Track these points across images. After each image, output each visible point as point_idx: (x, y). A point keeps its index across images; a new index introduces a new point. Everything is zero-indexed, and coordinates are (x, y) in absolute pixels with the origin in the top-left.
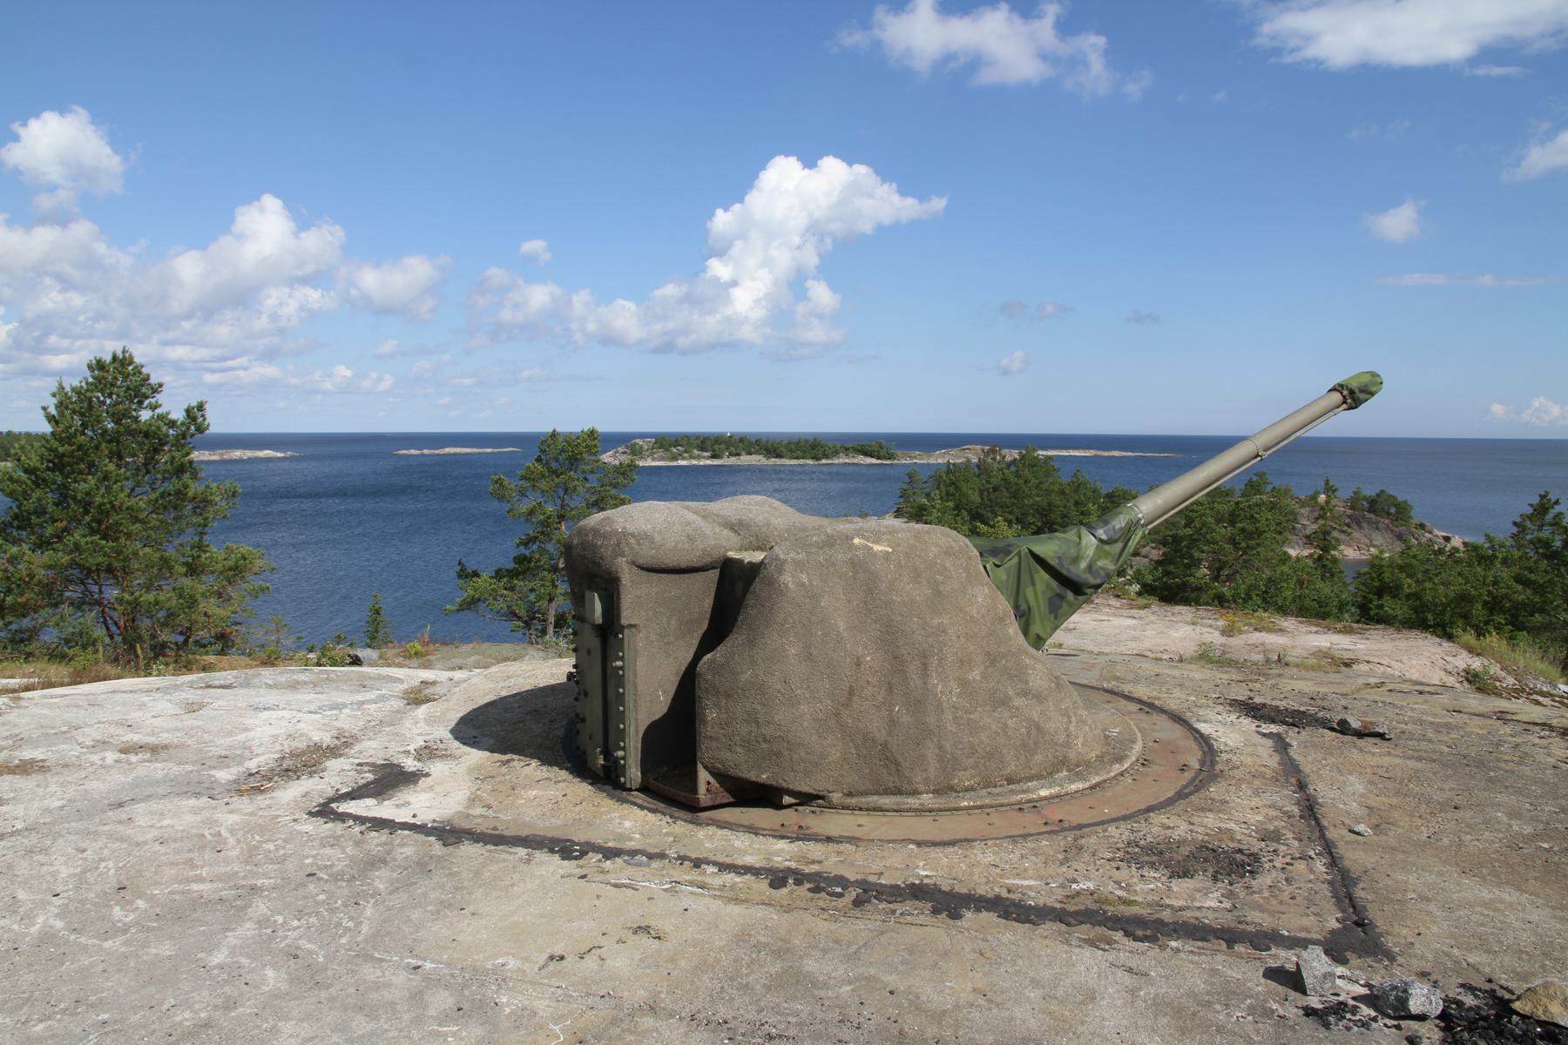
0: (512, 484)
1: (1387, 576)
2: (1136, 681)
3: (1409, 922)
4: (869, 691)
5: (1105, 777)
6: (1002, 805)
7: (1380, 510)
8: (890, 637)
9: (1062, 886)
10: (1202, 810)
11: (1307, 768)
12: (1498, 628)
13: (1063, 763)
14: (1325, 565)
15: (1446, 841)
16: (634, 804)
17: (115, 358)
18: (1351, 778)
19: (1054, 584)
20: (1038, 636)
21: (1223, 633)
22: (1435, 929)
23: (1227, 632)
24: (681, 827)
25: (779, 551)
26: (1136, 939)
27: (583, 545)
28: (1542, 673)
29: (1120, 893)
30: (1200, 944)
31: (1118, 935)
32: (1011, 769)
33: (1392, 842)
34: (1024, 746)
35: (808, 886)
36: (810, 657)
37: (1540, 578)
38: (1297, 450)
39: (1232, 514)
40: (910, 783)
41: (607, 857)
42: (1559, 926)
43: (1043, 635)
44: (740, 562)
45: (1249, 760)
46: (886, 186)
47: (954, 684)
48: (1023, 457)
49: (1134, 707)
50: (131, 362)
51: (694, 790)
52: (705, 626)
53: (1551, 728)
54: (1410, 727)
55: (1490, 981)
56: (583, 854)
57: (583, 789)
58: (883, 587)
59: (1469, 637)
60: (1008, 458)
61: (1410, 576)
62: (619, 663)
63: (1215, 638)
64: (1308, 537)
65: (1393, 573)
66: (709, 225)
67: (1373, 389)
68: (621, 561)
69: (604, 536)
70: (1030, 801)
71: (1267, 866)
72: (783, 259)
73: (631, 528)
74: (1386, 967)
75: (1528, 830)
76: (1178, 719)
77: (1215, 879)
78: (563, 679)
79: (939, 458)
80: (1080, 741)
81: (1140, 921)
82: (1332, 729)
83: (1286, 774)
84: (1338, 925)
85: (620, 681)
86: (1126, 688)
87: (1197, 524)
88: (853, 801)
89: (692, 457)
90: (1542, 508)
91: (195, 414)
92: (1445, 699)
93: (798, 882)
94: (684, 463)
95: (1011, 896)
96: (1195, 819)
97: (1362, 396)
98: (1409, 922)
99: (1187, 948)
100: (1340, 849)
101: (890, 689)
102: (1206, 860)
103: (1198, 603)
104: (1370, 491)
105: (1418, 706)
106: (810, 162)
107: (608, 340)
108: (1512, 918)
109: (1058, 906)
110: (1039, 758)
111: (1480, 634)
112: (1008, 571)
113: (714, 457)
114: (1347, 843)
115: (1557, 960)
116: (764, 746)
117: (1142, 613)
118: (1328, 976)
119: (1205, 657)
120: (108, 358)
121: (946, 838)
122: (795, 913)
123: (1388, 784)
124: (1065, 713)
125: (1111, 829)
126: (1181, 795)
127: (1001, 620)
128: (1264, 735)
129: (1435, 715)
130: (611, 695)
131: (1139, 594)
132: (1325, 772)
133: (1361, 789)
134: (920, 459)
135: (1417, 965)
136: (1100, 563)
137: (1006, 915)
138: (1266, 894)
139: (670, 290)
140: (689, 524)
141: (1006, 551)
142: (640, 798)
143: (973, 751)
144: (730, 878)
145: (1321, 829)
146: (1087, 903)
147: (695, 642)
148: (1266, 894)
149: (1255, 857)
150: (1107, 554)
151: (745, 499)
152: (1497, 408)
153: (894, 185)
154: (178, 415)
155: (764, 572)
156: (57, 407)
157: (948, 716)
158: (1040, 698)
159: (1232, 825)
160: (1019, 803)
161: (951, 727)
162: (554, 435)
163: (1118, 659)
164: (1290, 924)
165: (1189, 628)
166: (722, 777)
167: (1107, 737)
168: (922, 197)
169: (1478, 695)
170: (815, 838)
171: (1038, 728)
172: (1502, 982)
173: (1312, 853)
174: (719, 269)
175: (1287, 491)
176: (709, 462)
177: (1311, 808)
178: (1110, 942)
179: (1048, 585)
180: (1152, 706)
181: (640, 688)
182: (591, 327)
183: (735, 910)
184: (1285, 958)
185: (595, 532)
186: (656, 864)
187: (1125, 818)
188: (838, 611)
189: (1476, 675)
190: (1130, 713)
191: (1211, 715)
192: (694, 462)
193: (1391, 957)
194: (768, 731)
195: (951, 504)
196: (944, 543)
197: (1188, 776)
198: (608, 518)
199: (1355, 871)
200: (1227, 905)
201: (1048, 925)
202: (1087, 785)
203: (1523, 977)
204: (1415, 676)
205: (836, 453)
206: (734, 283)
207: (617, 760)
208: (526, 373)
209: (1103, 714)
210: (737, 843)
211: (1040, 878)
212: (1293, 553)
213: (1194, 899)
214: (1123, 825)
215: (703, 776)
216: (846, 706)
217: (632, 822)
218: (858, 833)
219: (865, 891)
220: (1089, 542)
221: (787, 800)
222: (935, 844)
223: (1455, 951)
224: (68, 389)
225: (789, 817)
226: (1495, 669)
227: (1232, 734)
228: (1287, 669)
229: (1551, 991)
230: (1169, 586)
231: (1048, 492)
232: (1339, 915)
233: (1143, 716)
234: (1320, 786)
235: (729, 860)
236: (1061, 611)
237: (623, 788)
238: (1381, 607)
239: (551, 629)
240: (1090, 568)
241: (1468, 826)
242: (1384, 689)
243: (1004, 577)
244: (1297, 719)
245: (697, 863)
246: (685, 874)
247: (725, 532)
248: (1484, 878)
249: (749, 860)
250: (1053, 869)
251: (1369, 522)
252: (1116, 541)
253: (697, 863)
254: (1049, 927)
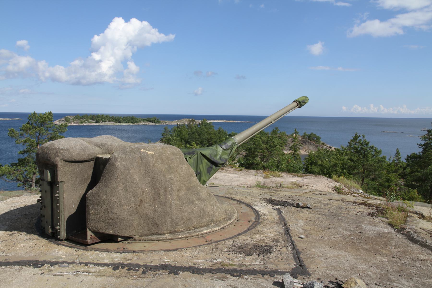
0: (17, 132)
1: (313, 159)
2: (236, 194)
3: (315, 264)
4: (147, 201)
5: (225, 225)
6: (192, 236)
7: (311, 139)
8: (154, 182)
9: (211, 261)
10: (255, 234)
11: (287, 219)
12: (344, 174)
13: (212, 221)
14: (295, 156)
15: (326, 238)
16: (63, 245)
18: (300, 221)
19: (209, 163)
20: (204, 180)
21: (264, 178)
22: (322, 265)
23: (265, 178)
24: (81, 252)
25: (116, 154)
26: (234, 276)
27: (43, 153)
28: (355, 187)
29: (229, 262)
30: (254, 276)
31: (229, 276)
32: (195, 224)
33: (311, 240)
35: (126, 268)
36: (126, 190)
37: (355, 159)
38: (284, 120)
39: (267, 140)
40: (162, 231)
41: (52, 266)
42: (355, 261)
43: (205, 180)
44: (102, 158)
45: (270, 217)
46: (154, 30)
47: (175, 197)
48: (202, 123)
49: (235, 202)
51: (86, 238)
52: (90, 181)
53: (356, 203)
54: (317, 205)
55: (337, 279)
56: (42, 265)
57: (44, 241)
58: (151, 165)
59: (335, 177)
60: (198, 123)
61: (319, 159)
62: (57, 195)
63: (262, 180)
64: (290, 147)
65: (315, 158)
66: (92, 40)
67: (306, 102)
68: (58, 159)
69: (51, 150)
70: (201, 234)
71: (274, 250)
72: (119, 53)
73: (61, 147)
74: (308, 278)
75: (348, 233)
76: (248, 205)
77: (259, 255)
78: (36, 202)
79: (175, 123)
80: (217, 214)
81: (235, 271)
82: (295, 206)
83: (281, 221)
84: (295, 267)
85: (58, 201)
86: (233, 196)
87: (257, 143)
88: (142, 238)
89: (88, 122)
90: (356, 138)
92: (327, 196)
93: (123, 267)
94: (86, 124)
95: (195, 266)
96: (253, 237)
97: (303, 104)
98: (315, 264)
99: (250, 278)
100: (296, 243)
101: (154, 200)
102: (256, 250)
103: (257, 169)
104: (309, 133)
105: (320, 198)
106: (127, 20)
107: (54, 79)
108: (343, 260)
109: (210, 268)
110: (204, 220)
111: (339, 176)
113: (97, 122)
114: (298, 241)
115: (354, 271)
116: (111, 221)
117: (239, 172)
118: (292, 282)
119: (258, 186)
121: (174, 248)
122: (121, 278)
123: (310, 222)
124: (212, 205)
125: (227, 242)
126: (249, 229)
127: (191, 175)
128: (275, 209)
129: (324, 201)
130: (54, 207)
131: (239, 166)
132: (292, 220)
133: (302, 224)
134: (169, 123)
135: (317, 276)
136: (223, 157)
137: (193, 272)
138: (274, 259)
139: (77, 62)
140: (83, 145)
141: (193, 153)
142: (66, 243)
143: (182, 219)
144: (99, 268)
145: (291, 237)
146: (220, 266)
147: (86, 186)
148: (274, 259)
149: (271, 247)
150: (226, 154)
151: (104, 136)
152: (344, 108)
153: (157, 30)
155: (110, 162)
157: (174, 208)
158: (204, 200)
159: (264, 238)
160: (198, 235)
161: (175, 211)
162: (34, 114)
163: (231, 187)
164: (281, 267)
165: (254, 177)
166: (96, 233)
167: (226, 212)
168: (166, 34)
169: (337, 194)
170: (129, 252)
171: (204, 210)
172: (340, 279)
173: (288, 245)
174: (96, 56)
175: (284, 133)
176: (95, 124)
177: (288, 231)
178: (226, 278)
179: (207, 164)
180: (240, 202)
181: (65, 203)
182: (47, 74)
183: (100, 279)
184: (278, 278)
185: (48, 148)
186: (71, 266)
187: (231, 238)
188: (136, 173)
189: (337, 188)
190: (234, 204)
191: (259, 204)
192: (89, 124)
193: (310, 275)
194: (112, 216)
195: (179, 138)
196: (174, 152)
197: (251, 223)
198: (53, 144)
199: (300, 250)
200: (262, 263)
201: (207, 274)
202: (220, 228)
203: (345, 277)
204: (320, 189)
205: (140, 121)
206: (100, 61)
207: (57, 230)
208: (22, 91)
209: (225, 205)
210: (101, 256)
211: (204, 259)
212: (286, 152)
213: (252, 262)
214: (231, 240)
215: (89, 233)
216: (139, 206)
217: (62, 251)
218: (144, 249)
219: (146, 268)
220: (220, 150)
221: (119, 239)
222: (170, 250)
223: (327, 271)
225: (120, 245)
226: (343, 186)
227: (265, 209)
228: (283, 189)
229: (352, 280)
230: (248, 165)
231: (210, 134)
232: (295, 263)
233: (238, 205)
234: (291, 224)
235: (98, 262)
236: (211, 172)
237: (59, 240)
238: (311, 169)
239: (34, 185)
240: (220, 158)
241: (332, 233)
242: (311, 193)
243: (192, 161)
244: (284, 204)
245: (86, 264)
246: (82, 268)
247: (97, 148)
248: (336, 249)
249: (106, 261)
250: (209, 256)
251: (308, 143)
252: (228, 149)
253: (86, 264)
254: (207, 275)
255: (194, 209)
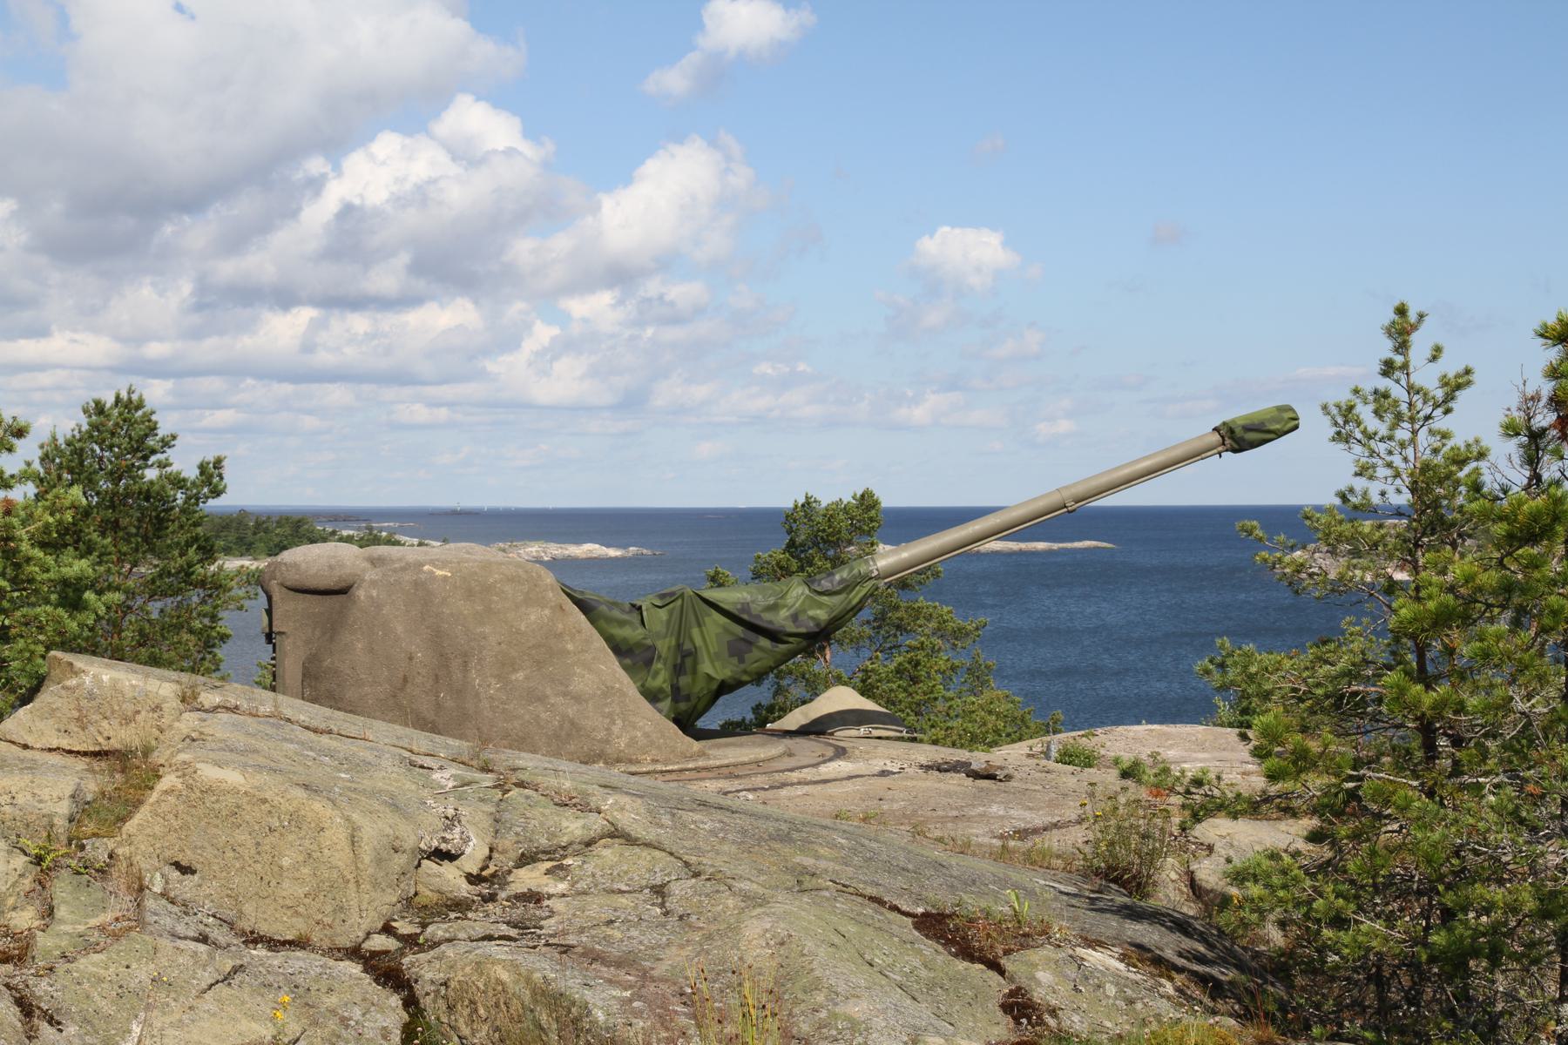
4: (419, 680)
8: (437, 639)
17: (118, 400)
34: (557, 737)
36: (371, 651)
50: (140, 406)
91: (211, 476)
112: (671, 613)
120: (109, 400)
154: (192, 473)
156: (42, 460)
157: (485, 704)
179: (726, 630)
224: (61, 441)
240: (795, 617)
255: (543, 716)
